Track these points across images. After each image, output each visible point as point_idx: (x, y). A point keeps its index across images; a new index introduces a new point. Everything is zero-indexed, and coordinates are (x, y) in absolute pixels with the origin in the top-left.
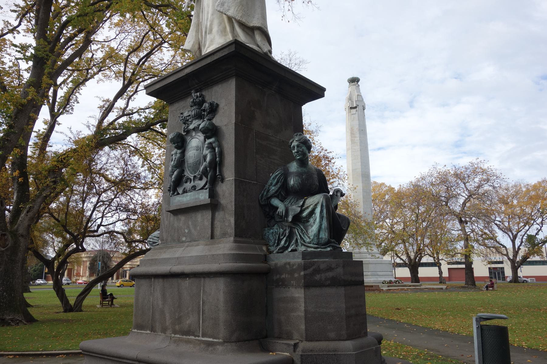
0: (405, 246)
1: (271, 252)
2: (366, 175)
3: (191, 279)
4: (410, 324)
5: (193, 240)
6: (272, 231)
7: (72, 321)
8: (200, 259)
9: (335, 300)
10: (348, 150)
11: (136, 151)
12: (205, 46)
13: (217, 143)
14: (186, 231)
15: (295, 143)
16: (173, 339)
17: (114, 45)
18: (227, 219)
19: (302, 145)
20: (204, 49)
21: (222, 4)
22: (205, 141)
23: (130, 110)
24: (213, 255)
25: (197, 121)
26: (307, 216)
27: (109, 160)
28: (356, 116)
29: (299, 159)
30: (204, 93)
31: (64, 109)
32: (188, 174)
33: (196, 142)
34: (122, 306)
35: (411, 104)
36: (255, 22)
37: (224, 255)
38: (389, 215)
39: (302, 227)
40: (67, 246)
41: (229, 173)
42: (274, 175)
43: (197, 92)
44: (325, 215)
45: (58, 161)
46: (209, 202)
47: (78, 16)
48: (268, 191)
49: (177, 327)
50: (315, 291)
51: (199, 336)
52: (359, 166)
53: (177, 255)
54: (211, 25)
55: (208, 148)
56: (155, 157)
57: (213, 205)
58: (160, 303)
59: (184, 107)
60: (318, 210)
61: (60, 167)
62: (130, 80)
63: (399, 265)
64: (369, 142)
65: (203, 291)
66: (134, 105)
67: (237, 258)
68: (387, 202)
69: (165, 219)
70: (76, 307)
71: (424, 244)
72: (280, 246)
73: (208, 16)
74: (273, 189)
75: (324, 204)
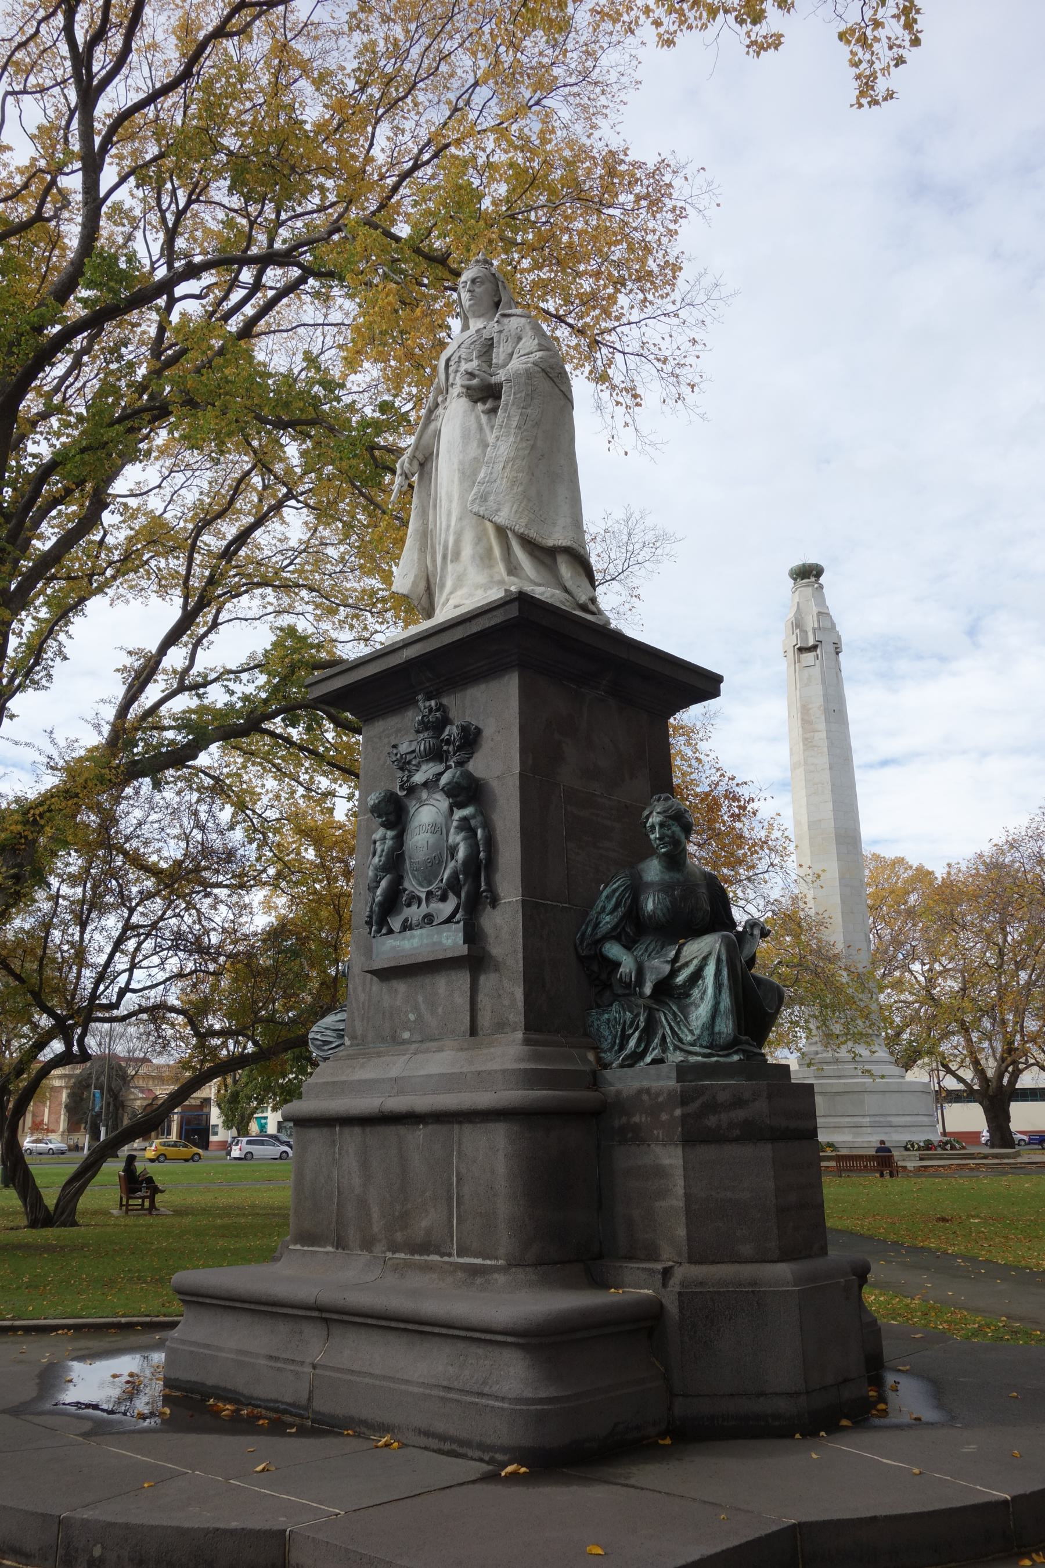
0: (969, 1040)
1: (606, 1066)
2: (847, 836)
3: (430, 1127)
4: (973, 1259)
5: (427, 1038)
6: (606, 1016)
7: (62, 1248)
8: (451, 1081)
9: (751, 1172)
10: (794, 767)
11: (219, 789)
12: (442, 586)
13: (479, 818)
14: (412, 1017)
15: (655, 819)
16: (390, 1263)
17: (155, 503)
18: (506, 992)
19: (671, 822)
20: (441, 592)
21: (484, 498)
22: (452, 812)
23: (199, 674)
24: (479, 1073)
25: (431, 765)
26: (685, 982)
27: (155, 820)
28: (816, 672)
29: (664, 854)
30: (445, 701)
31: (27, 675)
32: (411, 885)
33: (428, 814)
34: (179, 1213)
35: (972, 632)
36: (558, 538)
37: (504, 1071)
38: (920, 949)
39: (675, 1008)
40: (41, 1045)
41: (509, 886)
42: (608, 890)
43: (429, 699)
44: (726, 982)
45: (25, 823)
46: (466, 953)
47: (83, 451)
48: (596, 925)
49: (399, 1236)
50: (707, 1152)
51: (450, 1255)
52: (827, 811)
53: (394, 1072)
54: (458, 542)
55: (459, 829)
56: (265, 800)
57: (476, 960)
58: (357, 1181)
59: (399, 730)
60: (710, 971)
61: (30, 837)
62: (202, 597)
63: (955, 1097)
64: (855, 744)
65: (459, 1152)
66: (207, 660)
67: (531, 1078)
68: (910, 913)
69: (360, 989)
70: (62, 1214)
71: (1022, 1036)
72: (627, 1052)
73: (449, 520)
74: (608, 921)
75: (724, 957)
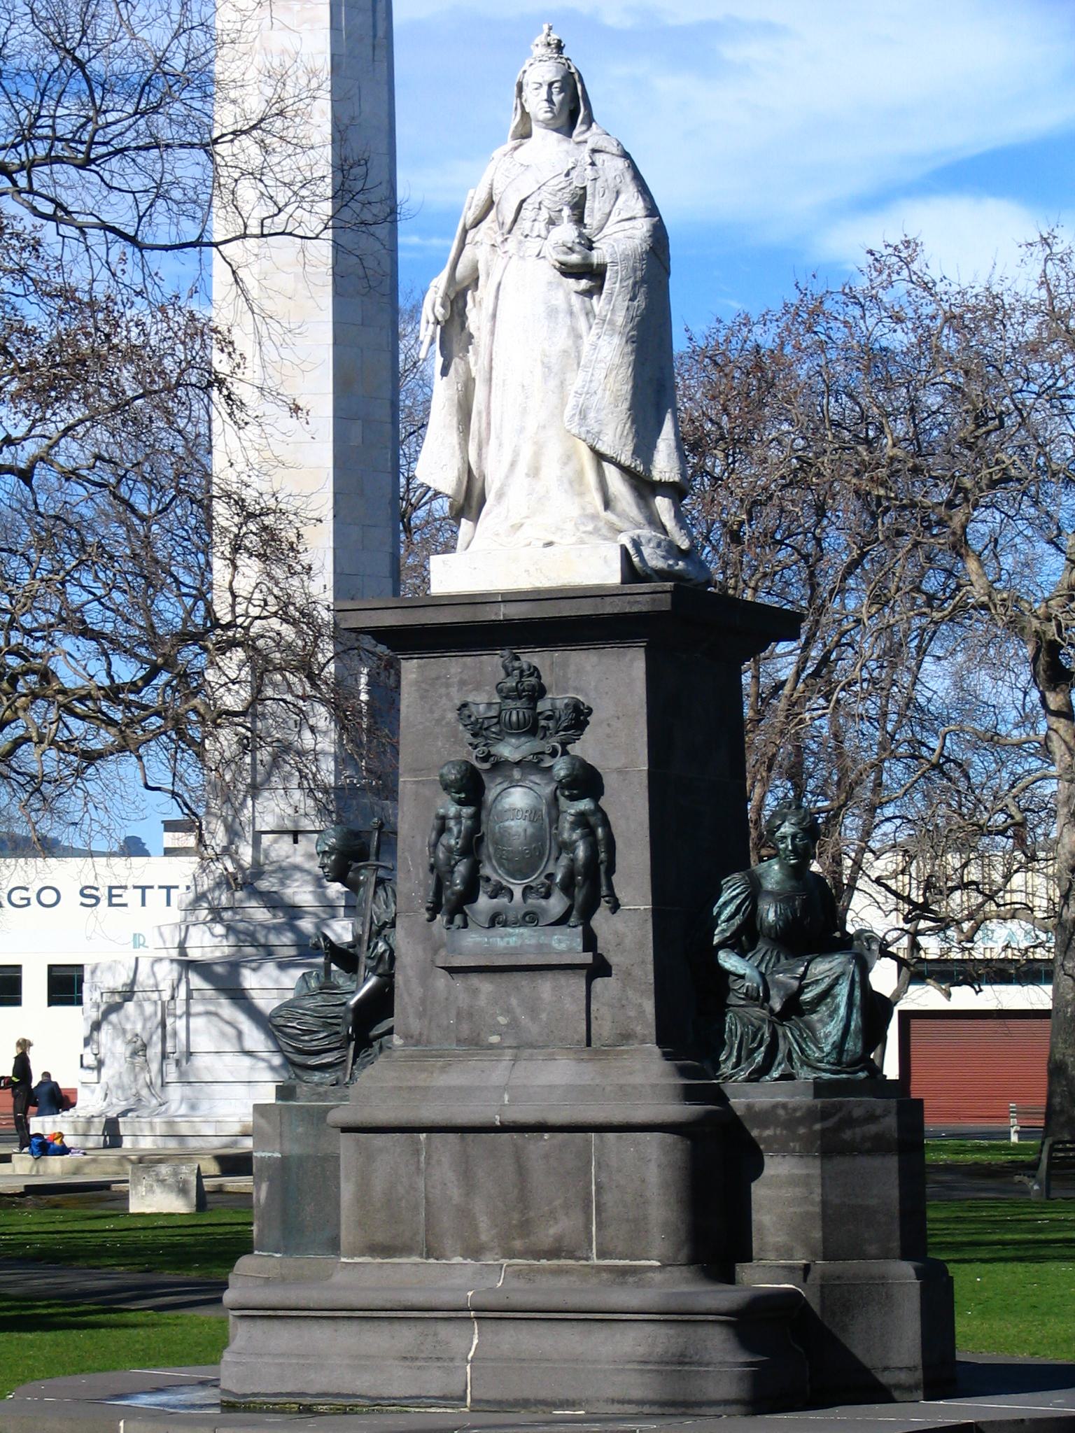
5: (523, 1047)
14: (502, 1020)
26: (813, 999)
29: (792, 866)
33: (516, 801)
37: (654, 1086)
50: (842, 1163)
51: (587, 1259)
58: (455, 1193)
75: (857, 979)
